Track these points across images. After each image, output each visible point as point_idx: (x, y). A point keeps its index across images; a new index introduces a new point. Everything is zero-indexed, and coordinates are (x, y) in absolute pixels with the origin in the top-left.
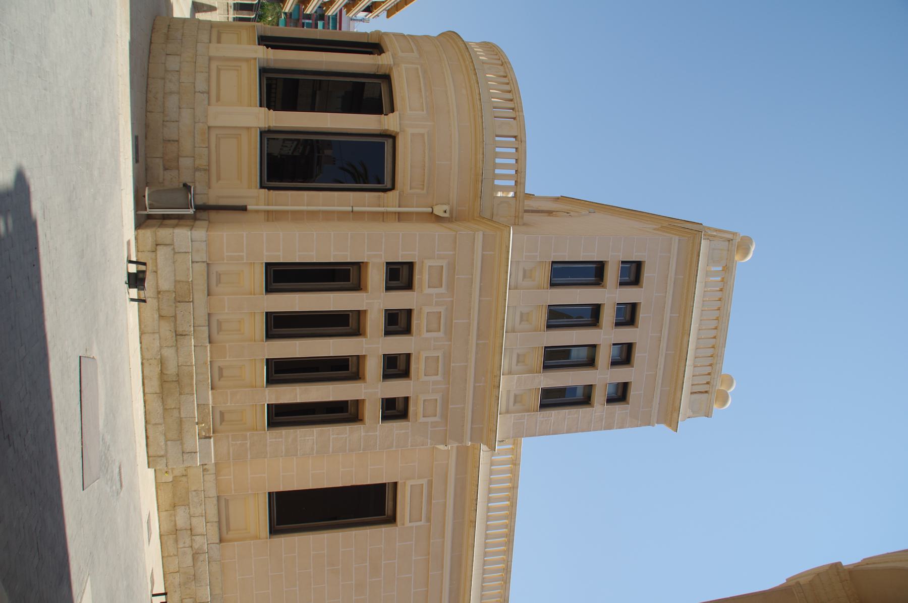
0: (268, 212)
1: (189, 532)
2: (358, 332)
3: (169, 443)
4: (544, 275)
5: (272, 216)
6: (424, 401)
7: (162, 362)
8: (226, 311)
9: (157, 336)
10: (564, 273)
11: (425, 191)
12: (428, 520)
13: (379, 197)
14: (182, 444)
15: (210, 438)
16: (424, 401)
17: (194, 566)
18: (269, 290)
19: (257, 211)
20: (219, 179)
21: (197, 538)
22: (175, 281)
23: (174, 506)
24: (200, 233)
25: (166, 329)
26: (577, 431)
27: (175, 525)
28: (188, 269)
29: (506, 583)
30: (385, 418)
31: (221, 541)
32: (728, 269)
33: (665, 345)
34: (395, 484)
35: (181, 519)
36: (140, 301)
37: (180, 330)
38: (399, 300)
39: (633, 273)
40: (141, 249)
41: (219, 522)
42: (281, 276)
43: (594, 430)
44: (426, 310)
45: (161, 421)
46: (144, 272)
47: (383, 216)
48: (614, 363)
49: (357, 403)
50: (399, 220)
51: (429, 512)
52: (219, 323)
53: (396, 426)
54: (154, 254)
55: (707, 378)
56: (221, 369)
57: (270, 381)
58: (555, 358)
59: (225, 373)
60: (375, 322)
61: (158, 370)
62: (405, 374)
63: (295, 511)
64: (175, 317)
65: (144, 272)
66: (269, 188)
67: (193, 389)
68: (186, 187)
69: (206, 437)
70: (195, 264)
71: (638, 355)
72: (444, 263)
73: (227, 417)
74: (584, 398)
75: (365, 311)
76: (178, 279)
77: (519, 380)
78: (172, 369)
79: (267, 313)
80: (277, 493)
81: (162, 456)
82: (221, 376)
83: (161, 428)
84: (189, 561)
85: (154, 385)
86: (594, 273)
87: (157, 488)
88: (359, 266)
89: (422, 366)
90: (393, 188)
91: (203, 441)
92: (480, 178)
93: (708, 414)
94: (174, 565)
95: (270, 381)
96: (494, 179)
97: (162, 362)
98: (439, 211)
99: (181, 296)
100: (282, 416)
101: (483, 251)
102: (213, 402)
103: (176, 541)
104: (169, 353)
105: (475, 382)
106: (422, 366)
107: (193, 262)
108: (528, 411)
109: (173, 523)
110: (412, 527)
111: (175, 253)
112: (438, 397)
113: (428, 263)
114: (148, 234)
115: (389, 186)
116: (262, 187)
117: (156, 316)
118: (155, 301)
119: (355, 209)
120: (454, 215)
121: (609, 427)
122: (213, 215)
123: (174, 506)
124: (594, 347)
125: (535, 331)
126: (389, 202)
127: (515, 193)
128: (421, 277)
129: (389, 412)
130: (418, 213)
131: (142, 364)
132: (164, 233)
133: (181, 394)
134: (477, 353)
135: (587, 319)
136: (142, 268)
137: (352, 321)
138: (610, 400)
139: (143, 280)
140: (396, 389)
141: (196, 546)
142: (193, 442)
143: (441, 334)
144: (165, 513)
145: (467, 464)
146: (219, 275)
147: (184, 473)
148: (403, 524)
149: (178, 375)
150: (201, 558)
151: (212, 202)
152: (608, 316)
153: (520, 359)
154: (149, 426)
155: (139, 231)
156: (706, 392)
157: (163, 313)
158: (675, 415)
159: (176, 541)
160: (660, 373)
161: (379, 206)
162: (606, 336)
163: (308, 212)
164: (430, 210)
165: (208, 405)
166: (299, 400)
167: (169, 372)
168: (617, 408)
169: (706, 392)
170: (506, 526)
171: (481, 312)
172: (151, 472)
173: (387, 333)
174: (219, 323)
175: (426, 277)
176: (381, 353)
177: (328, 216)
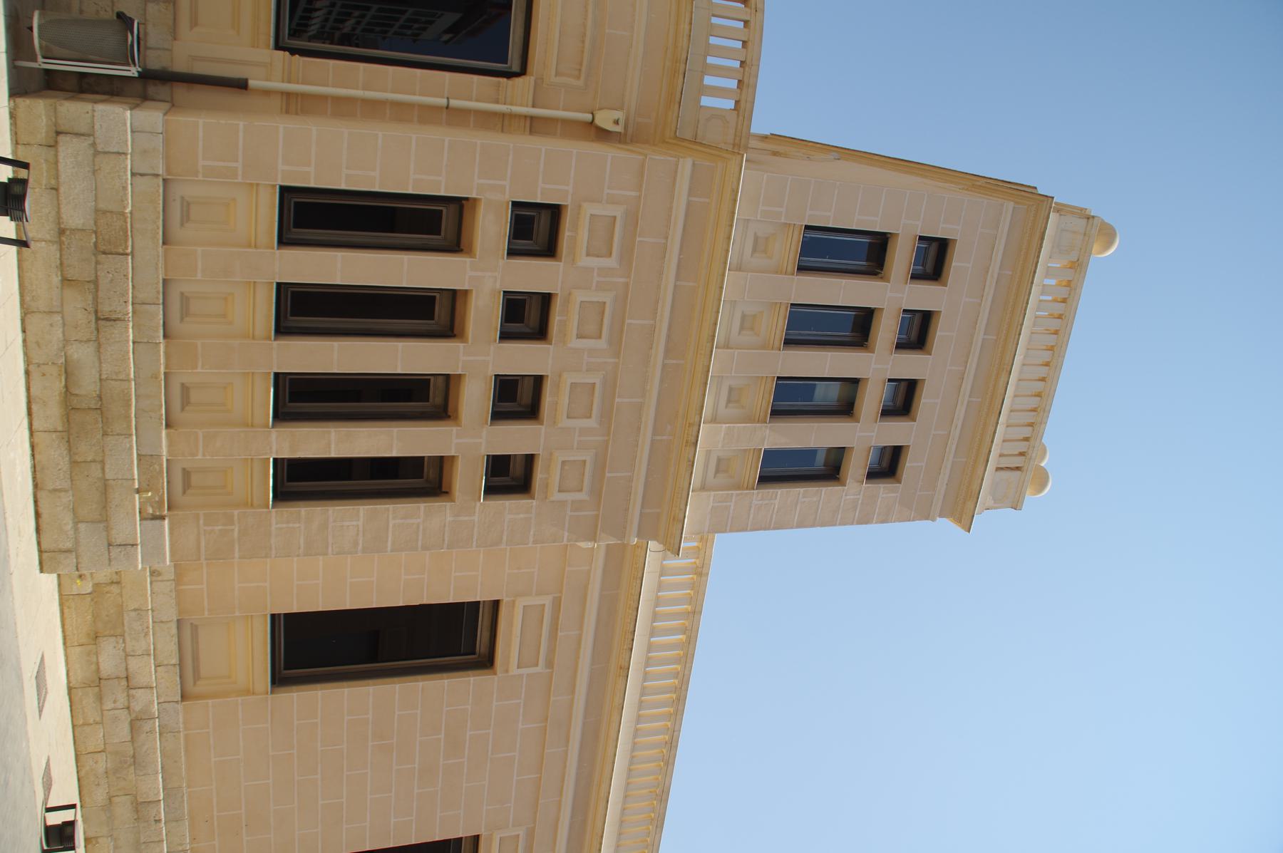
0: (288, 95)
1: (124, 683)
2: (450, 330)
3: (82, 526)
4: (788, 248)
5: (295, 104)
6: (563, 462)
7: (68, 371)
8: (199, 276)
9: (58, 318)
10: (825, 249)
11: (581, 83)
12: (550, 664)
13: (499, 84)
14: (108, 529)
15: (163, 518)
16: (563, 462)
17: (133, 740)
18: (283, 241)
19: (267, 93)
20: (194, 23)
21: (138, 693)
22: (97, 211)
23: (96, 637)
24: (152, 117)
25: (77, 306)
26: (813, 526)
27: (98, 669)
28: (125, 188)
29: (667, 764)
30: (491, 490)
31: (184, 697)
32: (1078, 266)
33: (969, 388)
34: (496, 604)
35: (109, 660)
36: (21, 243)
37: (105, 309)
38: (531, 275)
39: (934, 259)
40: (23, 138)
41: (181, 664)
42: (312, 214)
43: (843, 523)
44: (580, 296)
45: (67, 485)
46: (24, 183)
47: (501, 122)
48: (887, 413)
49: (441, 463)
50: (532, 131)
51: (551, 651)
52: (185, 299)
53: (509, 506)
54: (52, 151)
55: (1022, 447)
56: (185, 389)
57: (281, 416)
58: (792, 399)
59: (194, 396)
60: (483, 313)
61: (59, 385)
62: (531, 412)
63: (318, 647)
64: (96, 282)
65: (24, 183)
66: (293, 51)
67: (129, 427)
68: (124, 20)
69: (154, 518)
70: (138, 179)
71: (925, 402)
72: (618, 211)
73: (195, 479)
74: (830, 468)
75: (466, 293)
76: (102, 206)
77: (731, 433)
78: (87, 385)
79: (279, 285)
80: (289, 616)
81: (68, 551)
82: (186, 402)
83: (67, 498)
84: (124, 731)
85: (51, 415)
86: (872, 252)
87: (61, 605)
88: (460, 206)
89: (564, 400)
90: (523, 72)
91: (149, 523)
92: (680, 70)
93: (1016, 506)
94: (95, 740)
95: (281, 416)
96: (703, 73)
97: (68, 371)
98: (605, 120)
99: (107, 242)
100: (301, 481)
101: (690, 194)
102: (169, 452)
103: (100, 698)
104: (82, 353)
105: (655, 432)
106: (564, 400)
107: (133, 174)
108: (738, 487)
109: (94, 667)
110: (521, 676)
111: (96, 153)
112: (588, 456)
113: (589, 209)
114: (38, 108)
115: (516, 68)
116: (278, 47)
117: (56, 280)
118: (54, 248)
119: (454, 103)
120: (630, 130)
121: (865, 520)
122: (180, 91)
123: (96, 637)
124: (855, 382)
125: (763, 347)
126: (515, 96)
127: (737, 103)
128: (574, 234)
129: (498, 480)
130: (565, 122)
131: (27, 373)
132: (74, 110)
133: (105, 434)
134: (662, 381)
135: (846, 334)
136: (23, 174)
137: (440, 310)
138: (873, 475)
139: (21, 198)
140: (514, 439)
141: (137, 707)
142: (130, 525)
143: (602, 344)
144: (78, 649)
145: (622, 573)
146: (186, 206)
147: (115, 578)
148: (507, 671)
149: (100, 397)
150: (147, 727)
151: (181, 66)
152: (886, 330)
153: (734, 396)
154: (41, 494)
155: (20, 100)
156: (1018, 468)
157: (71, 273)
158: (970, 505)
159: (100, 698)
160: (956, 433)
161: (497, 102)
162: (877, 365)
163: (365, 102)
164: (588, 117)
165: (160, 456)
166: (333, 454)
167: (82, 392)
168: (882, 489)
169: (1018, 468)
170: (676, 675)
171: (669, 311)
172: (49, 582)
173: (505, 336)
174: (185, 299)
175: (583, 235)
176: (493, 370)
177: (401, 112)
